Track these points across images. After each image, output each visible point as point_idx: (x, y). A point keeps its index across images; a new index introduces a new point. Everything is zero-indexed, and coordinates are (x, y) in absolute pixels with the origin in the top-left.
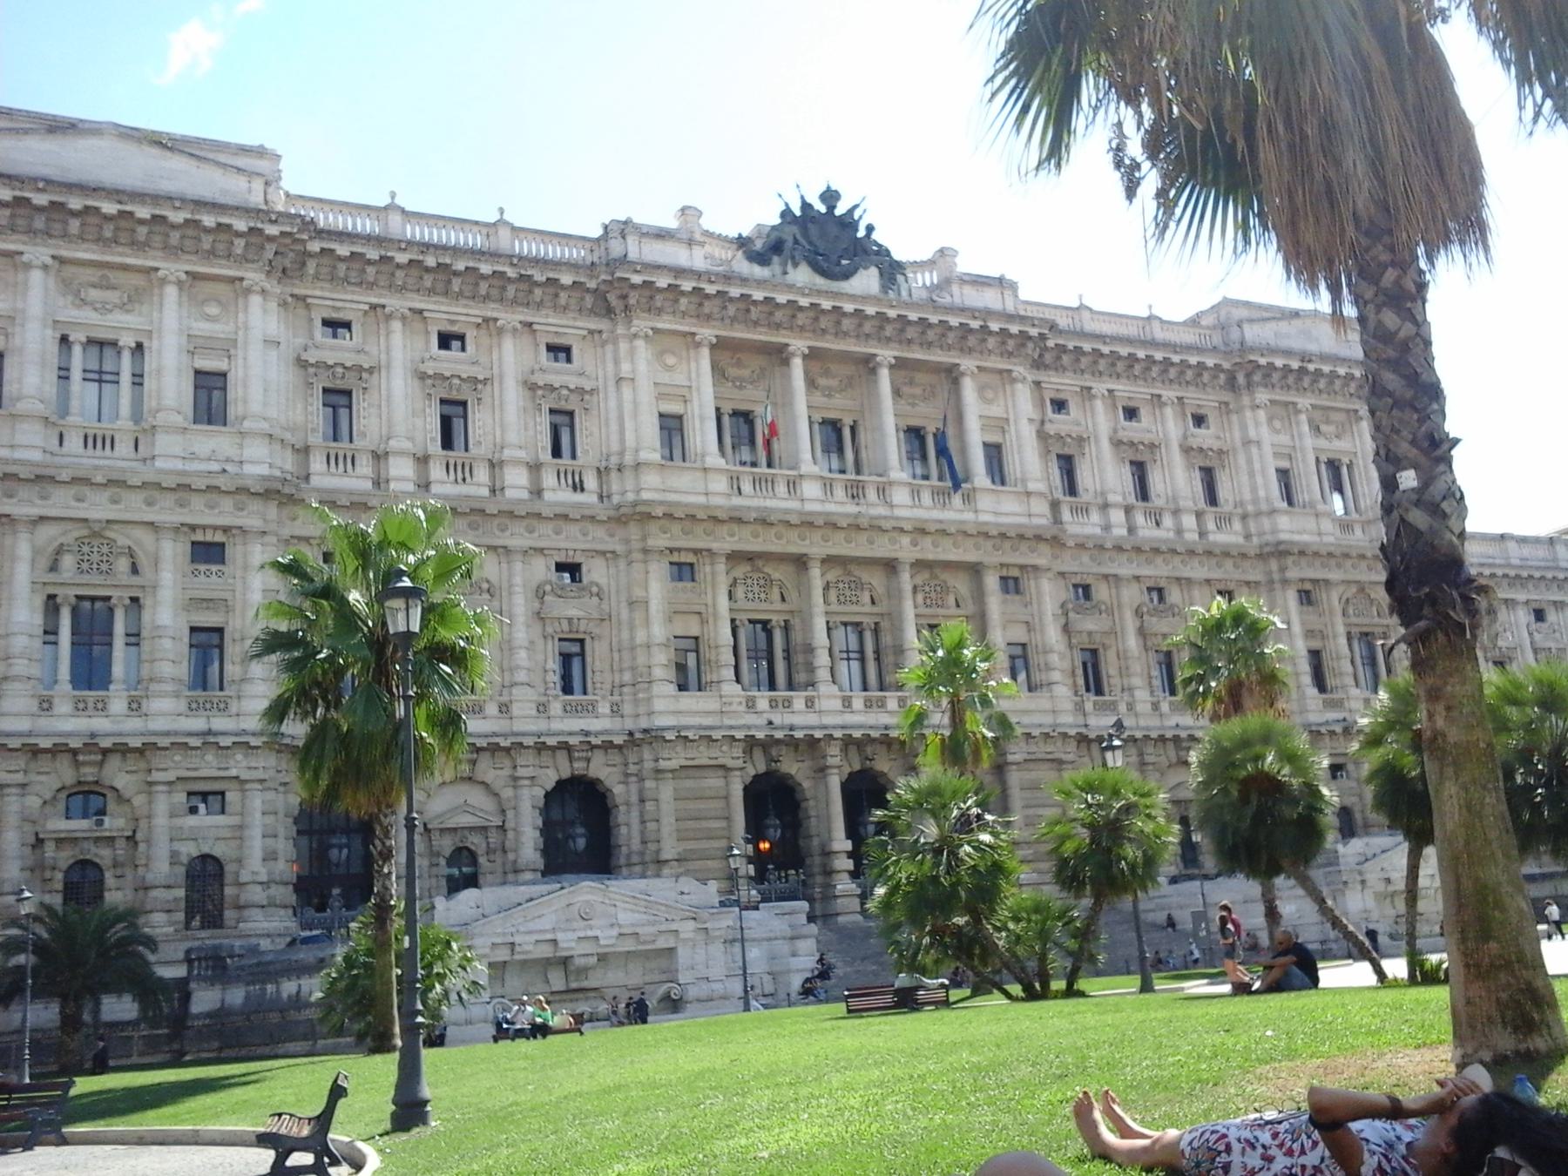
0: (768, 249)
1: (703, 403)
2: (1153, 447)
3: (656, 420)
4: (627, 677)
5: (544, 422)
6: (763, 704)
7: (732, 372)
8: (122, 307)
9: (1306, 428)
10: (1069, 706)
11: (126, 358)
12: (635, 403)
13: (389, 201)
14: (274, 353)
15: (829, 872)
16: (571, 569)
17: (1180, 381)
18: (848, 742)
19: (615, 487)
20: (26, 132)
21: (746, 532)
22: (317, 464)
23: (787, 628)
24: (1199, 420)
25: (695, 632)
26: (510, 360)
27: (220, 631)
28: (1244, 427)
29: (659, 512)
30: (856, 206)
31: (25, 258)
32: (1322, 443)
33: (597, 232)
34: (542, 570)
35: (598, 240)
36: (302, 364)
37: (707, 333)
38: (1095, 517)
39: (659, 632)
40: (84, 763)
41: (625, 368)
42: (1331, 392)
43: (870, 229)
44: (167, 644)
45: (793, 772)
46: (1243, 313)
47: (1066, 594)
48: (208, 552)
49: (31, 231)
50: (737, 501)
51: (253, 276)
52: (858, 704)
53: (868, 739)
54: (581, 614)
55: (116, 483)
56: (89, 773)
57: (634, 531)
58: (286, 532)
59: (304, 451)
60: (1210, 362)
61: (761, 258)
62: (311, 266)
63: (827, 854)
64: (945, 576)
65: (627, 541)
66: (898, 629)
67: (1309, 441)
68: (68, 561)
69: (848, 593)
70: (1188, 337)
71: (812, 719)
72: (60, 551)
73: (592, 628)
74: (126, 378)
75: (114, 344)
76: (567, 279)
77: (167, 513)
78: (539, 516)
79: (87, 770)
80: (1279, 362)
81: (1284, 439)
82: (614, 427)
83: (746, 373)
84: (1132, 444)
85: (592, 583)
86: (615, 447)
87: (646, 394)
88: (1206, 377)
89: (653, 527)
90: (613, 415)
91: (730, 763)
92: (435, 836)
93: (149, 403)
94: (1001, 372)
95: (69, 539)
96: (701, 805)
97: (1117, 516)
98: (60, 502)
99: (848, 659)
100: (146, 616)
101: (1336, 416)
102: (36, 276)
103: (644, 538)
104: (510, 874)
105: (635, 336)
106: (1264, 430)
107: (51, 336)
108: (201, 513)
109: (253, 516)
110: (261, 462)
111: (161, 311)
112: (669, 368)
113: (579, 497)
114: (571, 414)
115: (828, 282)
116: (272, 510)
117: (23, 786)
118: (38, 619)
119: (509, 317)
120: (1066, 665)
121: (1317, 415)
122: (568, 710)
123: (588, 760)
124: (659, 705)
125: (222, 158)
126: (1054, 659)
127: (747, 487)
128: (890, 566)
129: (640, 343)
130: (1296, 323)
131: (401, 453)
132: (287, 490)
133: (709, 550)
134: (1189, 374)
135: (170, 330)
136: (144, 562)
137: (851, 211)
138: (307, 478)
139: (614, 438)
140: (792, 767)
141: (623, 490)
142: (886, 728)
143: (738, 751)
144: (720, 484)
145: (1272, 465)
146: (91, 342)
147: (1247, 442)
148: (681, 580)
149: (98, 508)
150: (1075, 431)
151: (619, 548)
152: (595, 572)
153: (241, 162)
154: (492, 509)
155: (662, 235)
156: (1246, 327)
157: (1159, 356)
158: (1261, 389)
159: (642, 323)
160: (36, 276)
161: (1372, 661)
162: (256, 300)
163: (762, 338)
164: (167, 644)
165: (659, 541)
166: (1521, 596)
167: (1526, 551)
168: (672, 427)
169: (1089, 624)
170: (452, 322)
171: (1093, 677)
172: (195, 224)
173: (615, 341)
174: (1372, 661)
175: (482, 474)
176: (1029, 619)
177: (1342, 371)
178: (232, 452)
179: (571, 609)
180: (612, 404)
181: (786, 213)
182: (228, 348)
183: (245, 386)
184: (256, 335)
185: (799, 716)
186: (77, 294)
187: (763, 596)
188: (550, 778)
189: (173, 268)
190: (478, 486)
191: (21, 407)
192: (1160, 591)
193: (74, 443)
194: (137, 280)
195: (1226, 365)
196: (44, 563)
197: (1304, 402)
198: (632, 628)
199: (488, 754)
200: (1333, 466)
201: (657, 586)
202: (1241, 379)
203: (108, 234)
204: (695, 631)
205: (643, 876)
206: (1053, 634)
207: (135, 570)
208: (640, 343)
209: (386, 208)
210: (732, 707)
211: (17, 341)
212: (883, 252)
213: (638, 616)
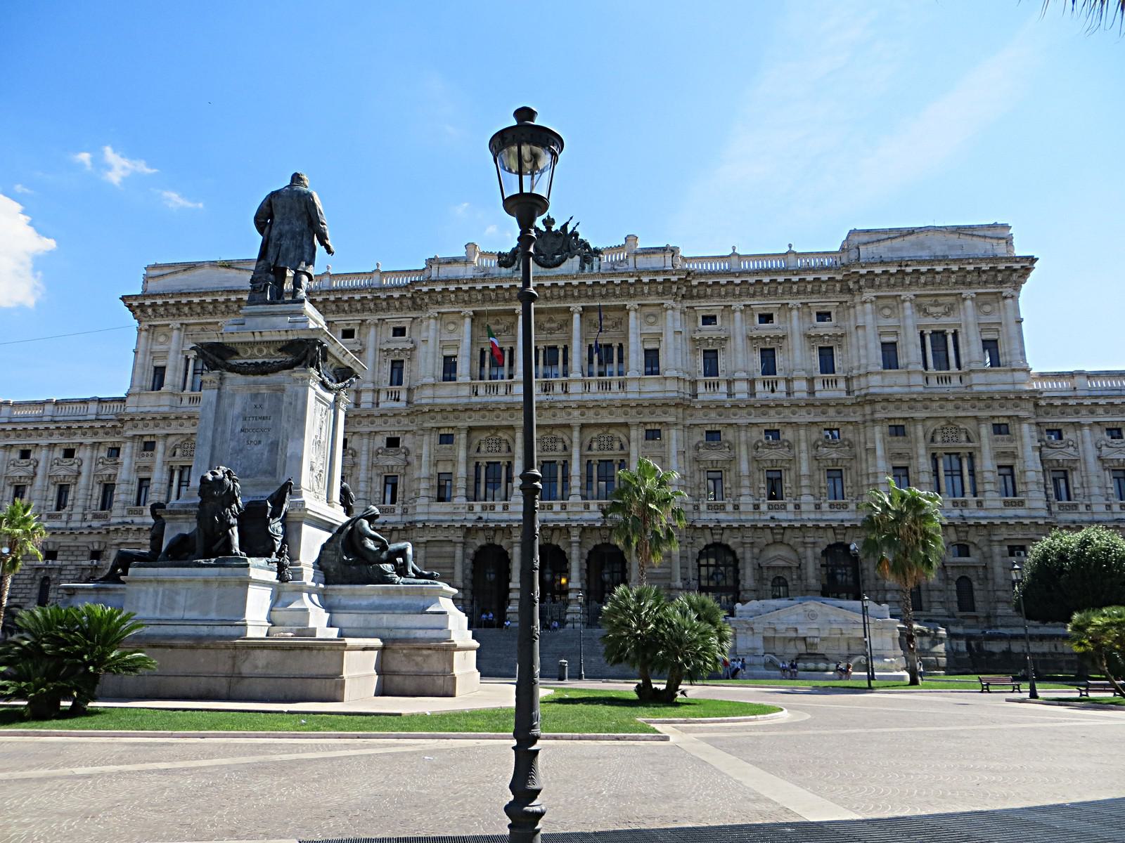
3: (642, 357)
6: (477, 508)
8: (946, 314)
13: (787, 249)
14: (679, 337)
16: (393, 442)
21: (476, 416)
22: (701, 388)
25: (449, 470)
26: (794, 325)
30: (568, 223)
31: (1004, 295)
34: (757, 435)
37: (468, 310)
40: (777, 534)
45: (730, 543)
46: (865, 238)
51: (669, 302)
52: (825, 506)
54: (778, 458)
56: (840, 538)
57: (868, 409)
58: (688, 422)
59: (694, 383)
64: (612, 431)
69: (550, 445)
71: (505, 516)
78: (813, 405)
79: (716, 537)
85: (784, 440)
86: (856, 364)
87: (871, 332)
89: (878, 407)
91: (455, 539)
92: (765, 570)
94: (995, 293)
96: (441, 561)
99: (952, 475)
100: (977, 462)
101: (941, 300)
103: (872, 413)
104: (806, 592)
107: (917, 333)
110: (671, 390)
111: (1006, 313)
112: (987, 314)
113: (396, 404)
115: (543, 269)
117: (814, 543)
123: (967, 532)
124: (419, 509)
127: (481, 391)
129: (432, 321)
130: (912, 238)
131: (741, 380)
132: (687, 403)
133: (1017, 416)
136: (972, 435)
138: (696, 396)
142: (842, 521)
143: (460, 533)
148: (897, 435)
150: (780, 333)
152: (406, 442)
153: (989, 233)
154: (376, 413)
155: (455, 261)
156: (862, 248)
158: (867, 290)
159: (433, 311)
163: (501, 308)
168: (450, 366)
170: (348, 324)
171: (775, 489)
172: (458, 289)
175: (782, 386)
176: (662, 454)
179: (392, 461)
182: (658, 337)
187: (955, 439)
190: (721, 394)
191: (667, 374)
195: (839, 277)
196: (168, 453)
197: (907, 294)
199: (974, 528)
203: (632, 292)
205: (848, 599)
207: (968, 440)
209: (786, 254)
210: (459, 509)
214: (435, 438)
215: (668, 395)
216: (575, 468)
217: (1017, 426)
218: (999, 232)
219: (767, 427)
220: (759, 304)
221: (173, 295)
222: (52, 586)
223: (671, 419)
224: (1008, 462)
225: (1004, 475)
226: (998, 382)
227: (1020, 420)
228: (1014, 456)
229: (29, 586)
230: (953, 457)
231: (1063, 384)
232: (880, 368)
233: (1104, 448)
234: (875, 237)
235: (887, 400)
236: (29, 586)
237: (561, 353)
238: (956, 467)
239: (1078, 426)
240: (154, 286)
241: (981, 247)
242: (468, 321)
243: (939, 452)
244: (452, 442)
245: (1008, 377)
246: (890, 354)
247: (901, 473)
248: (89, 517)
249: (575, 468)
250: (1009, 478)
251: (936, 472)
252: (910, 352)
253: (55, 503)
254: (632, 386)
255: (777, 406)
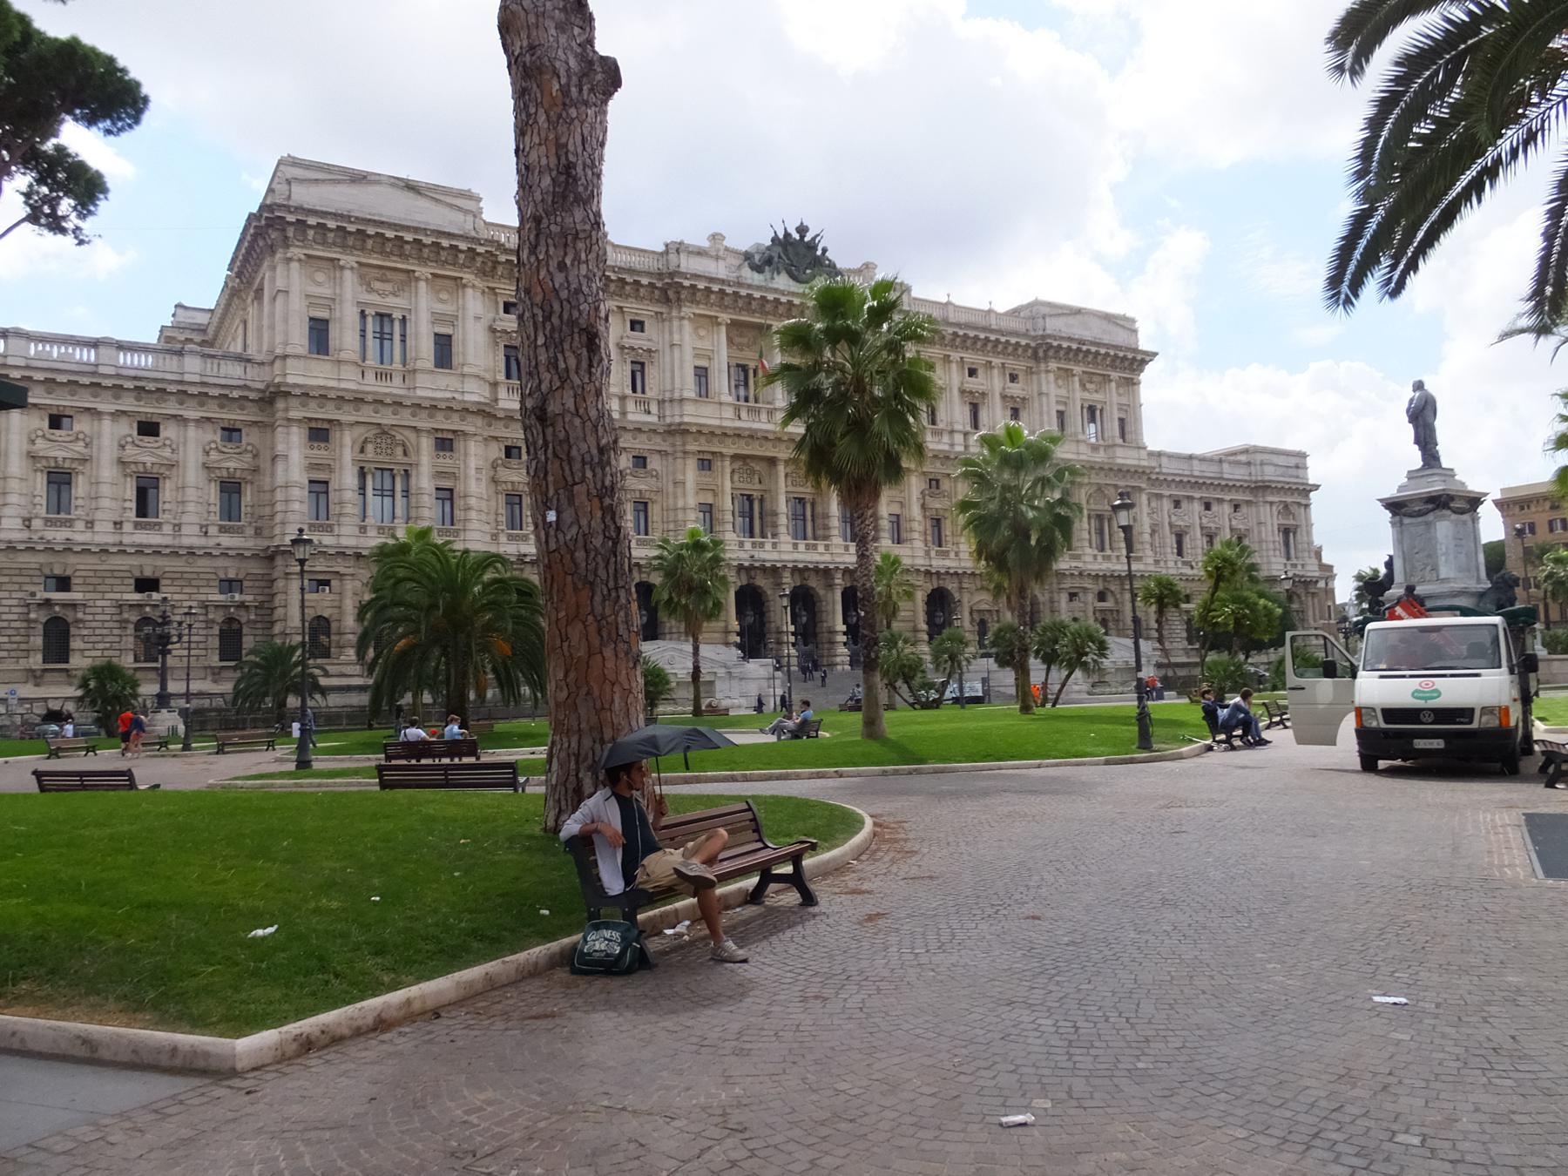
0: (762, 261)
1: (721, 357)
2: (983, 394)
4: (672, 526)
5: (628, 368)
6: (748, 546)
7: (737, 340)
9: (1077, 385)
10: (922, 553)
11: (397, 325)
12: (682, 361)
15: (832, 643)
17: (1004, 353)
18: (795, 570)
19: (668, 413)
20: (338, 182)
23: (762, 501)
24: (1013, 378)
27: (451, 490)
28: (1040, 384)
29: (694, 429)
32: (1086, 395)
33: (661, 248)
35: (661, 254)
36: (492, 330)
37: (725, 317)
38: (946, 438)
39: (692, 501)
41: (676, 338)
42: (1095, 363)
43: (825, 250)
44: (426, 498)
46: (1046, 310)
47: (924, 486)
48: (445, 444)
49: (344, 246)
50: (738, 424)
51: (468, 277)
52: (933, 554)
53: (806, 569)
55: (398, 404)
57: (678, 440)
58: (486, 434)
60: (1023, 342)
61: (758, 269)
62: (500, 270)
63: (833, 632)
65: (674, 445)
66: (775, 500)
67: (1079, 394)
68: (370, 447)
70: (1013, 324)
71: (775, 556)
72: (365, 441)
73: (652, 496)
74: (397, 337)
75: (390, 316)
76: (645, 281)
77: (424, 423)
80: (1065, 345)
81: (1063, 392)
82: (668, 374)
83: (745, 340)
84: (971, 392)
86: (668, 387)
88: (1020, 351)
89: (689, 438)
90: (668, 367)
93: (410, 354)
94: (456, 278)
95: (370, 435)
97: (959, 438)
98: (366, 415)
100: (413, 481)
101: (1095, 379)
102: (348, 273)
105: (683, 318)
106: (1052, 386)
107: (356, 310)
108: (441, 422)
109: (472, 425)
110: (475, 393)
112: (701, 338)
114: (642, 364)
115: (792, 282)
116: (479, 421)
118: (356, 482)
119: (424, 270)
120: (921, 528)
121: (1086, 377)
122: (511, 538)
125: (449, 200)
126: (915, 525)
127: (744, 414)
128: (772, 461)
134: (1010, 349)
135: (423, 308)
137: (814, 239)
138: (496, 400)
139: (668, 381)
140: (761, 581)
141: (673, 416)
144: (729, 413)
145: (1055, 408)
146: (378, 314)
147: (1040, 394)
149: (386, 417)
150: (981, 388)
151: (669, 449)
152: (654, 463)
155: (700, 253)
157: (993, 337)
159: (688, 310)
160: (348, 273)
161: (1101, 532)
162: (469, 291)
164: (426, 498)
165: (692, 447)
166: (1197, 495)
167: (1204, 467)
168: (702, 374)
169: (936, 504)
173: (670, 320)
174: (1101, 532)
177: (1103, 351)
178: (458, 386)
180: (667, 359)
181: (775, 240)
182: (452, 320)
183: (416, 338)
184: (471, 313)
185: (768, 554)
186: (369, 284)
188: (929, 587)
189: (424, 271)
191: (343, 356)
192: (937, 481)
193: (370, 377)
194: (403, 277)
195: (659, 285)
196: (357, 448)
197: (1078, 369)
198: (675, 497)
200: (1092, 410)
201: (690, 473)
202: (1041, 354)
204: (897, 512)
206: (916, 511)
207: (405, 454)
208: (686, 322)
211: (338, 314)
212: (832, 266)
213: (679, 491)
214: (305, 432)
215: (343, 385)
216: (782, 507)
217: (338, 434)
218: (1126, 324)
219: (55, 412)
220: (971, 357)
221: (335, 216)
222: (73, 631)
223: (470, 429)
224: (447, 484)
225: (318, 493)
226: (1125, 457)
227: (1140, 489)
228: (329, 468)
229: (116, 632)
230: (387, 474)
231: (88, 355)
232: (303, 351)
233: (39, 441)
234: (449, 200)
235: (751, 437)
236: (116, 632)
237: (397, 325)
238: (387, 485)
239: (94, 413)
240: (304, 196)
241: (1120, 338)
242: (723, 329)
243: (367, 466)
244: (327, 440)
245: (1134, 453)
246: (320, 333)
247: (320, 488)
248: (213, 530)
249: (782, 507)
250: (448, 504)
251: (363, 488)
252: (345, 337)
253: (133, 505)
254: (422, 380)
255: (376, 401)
